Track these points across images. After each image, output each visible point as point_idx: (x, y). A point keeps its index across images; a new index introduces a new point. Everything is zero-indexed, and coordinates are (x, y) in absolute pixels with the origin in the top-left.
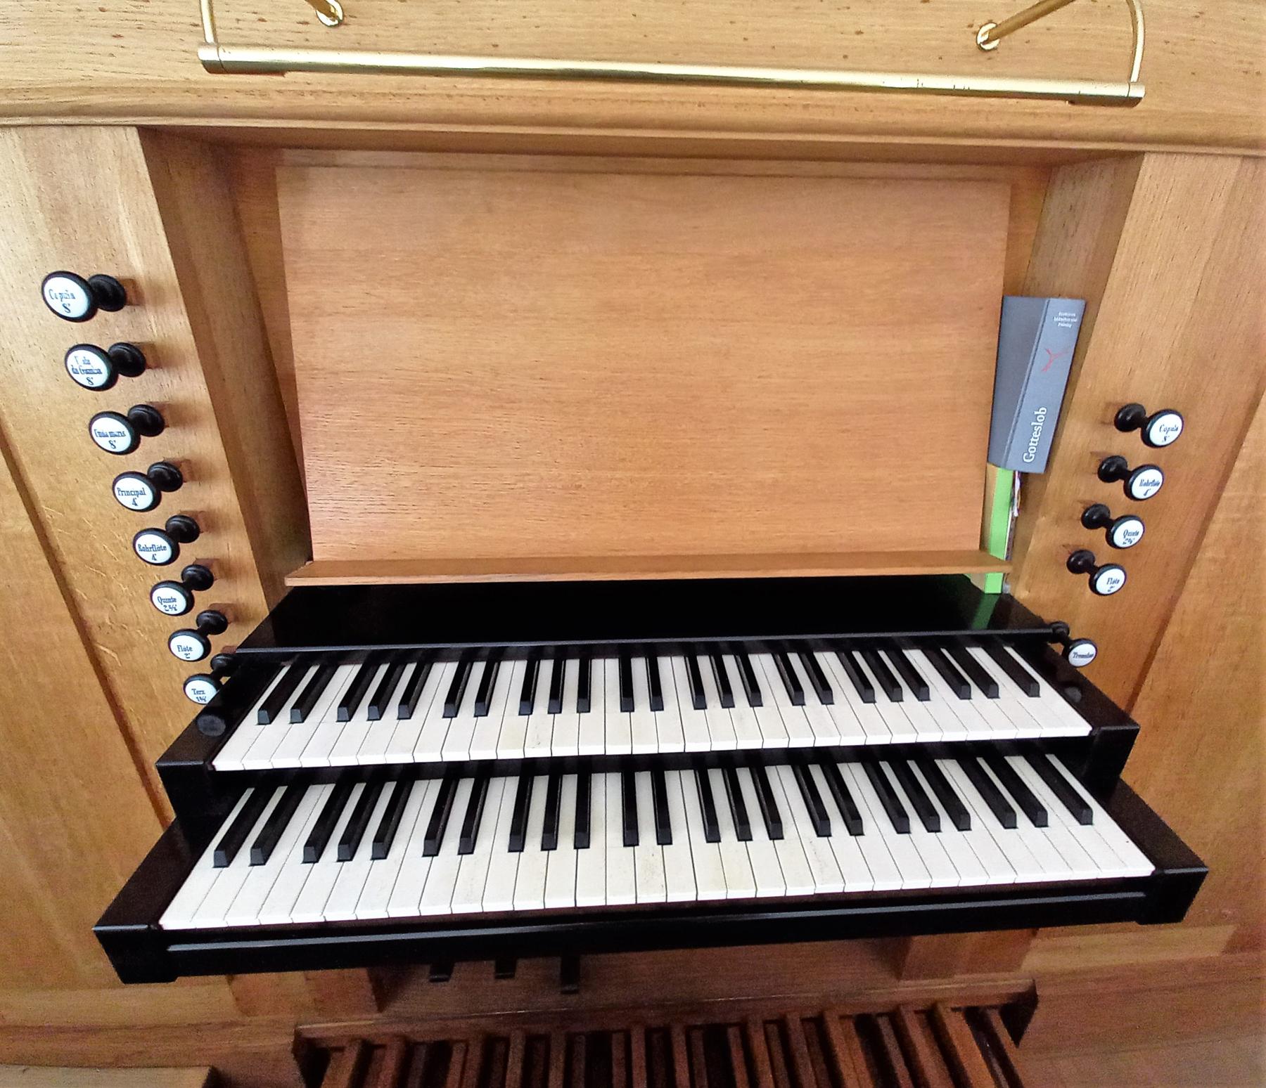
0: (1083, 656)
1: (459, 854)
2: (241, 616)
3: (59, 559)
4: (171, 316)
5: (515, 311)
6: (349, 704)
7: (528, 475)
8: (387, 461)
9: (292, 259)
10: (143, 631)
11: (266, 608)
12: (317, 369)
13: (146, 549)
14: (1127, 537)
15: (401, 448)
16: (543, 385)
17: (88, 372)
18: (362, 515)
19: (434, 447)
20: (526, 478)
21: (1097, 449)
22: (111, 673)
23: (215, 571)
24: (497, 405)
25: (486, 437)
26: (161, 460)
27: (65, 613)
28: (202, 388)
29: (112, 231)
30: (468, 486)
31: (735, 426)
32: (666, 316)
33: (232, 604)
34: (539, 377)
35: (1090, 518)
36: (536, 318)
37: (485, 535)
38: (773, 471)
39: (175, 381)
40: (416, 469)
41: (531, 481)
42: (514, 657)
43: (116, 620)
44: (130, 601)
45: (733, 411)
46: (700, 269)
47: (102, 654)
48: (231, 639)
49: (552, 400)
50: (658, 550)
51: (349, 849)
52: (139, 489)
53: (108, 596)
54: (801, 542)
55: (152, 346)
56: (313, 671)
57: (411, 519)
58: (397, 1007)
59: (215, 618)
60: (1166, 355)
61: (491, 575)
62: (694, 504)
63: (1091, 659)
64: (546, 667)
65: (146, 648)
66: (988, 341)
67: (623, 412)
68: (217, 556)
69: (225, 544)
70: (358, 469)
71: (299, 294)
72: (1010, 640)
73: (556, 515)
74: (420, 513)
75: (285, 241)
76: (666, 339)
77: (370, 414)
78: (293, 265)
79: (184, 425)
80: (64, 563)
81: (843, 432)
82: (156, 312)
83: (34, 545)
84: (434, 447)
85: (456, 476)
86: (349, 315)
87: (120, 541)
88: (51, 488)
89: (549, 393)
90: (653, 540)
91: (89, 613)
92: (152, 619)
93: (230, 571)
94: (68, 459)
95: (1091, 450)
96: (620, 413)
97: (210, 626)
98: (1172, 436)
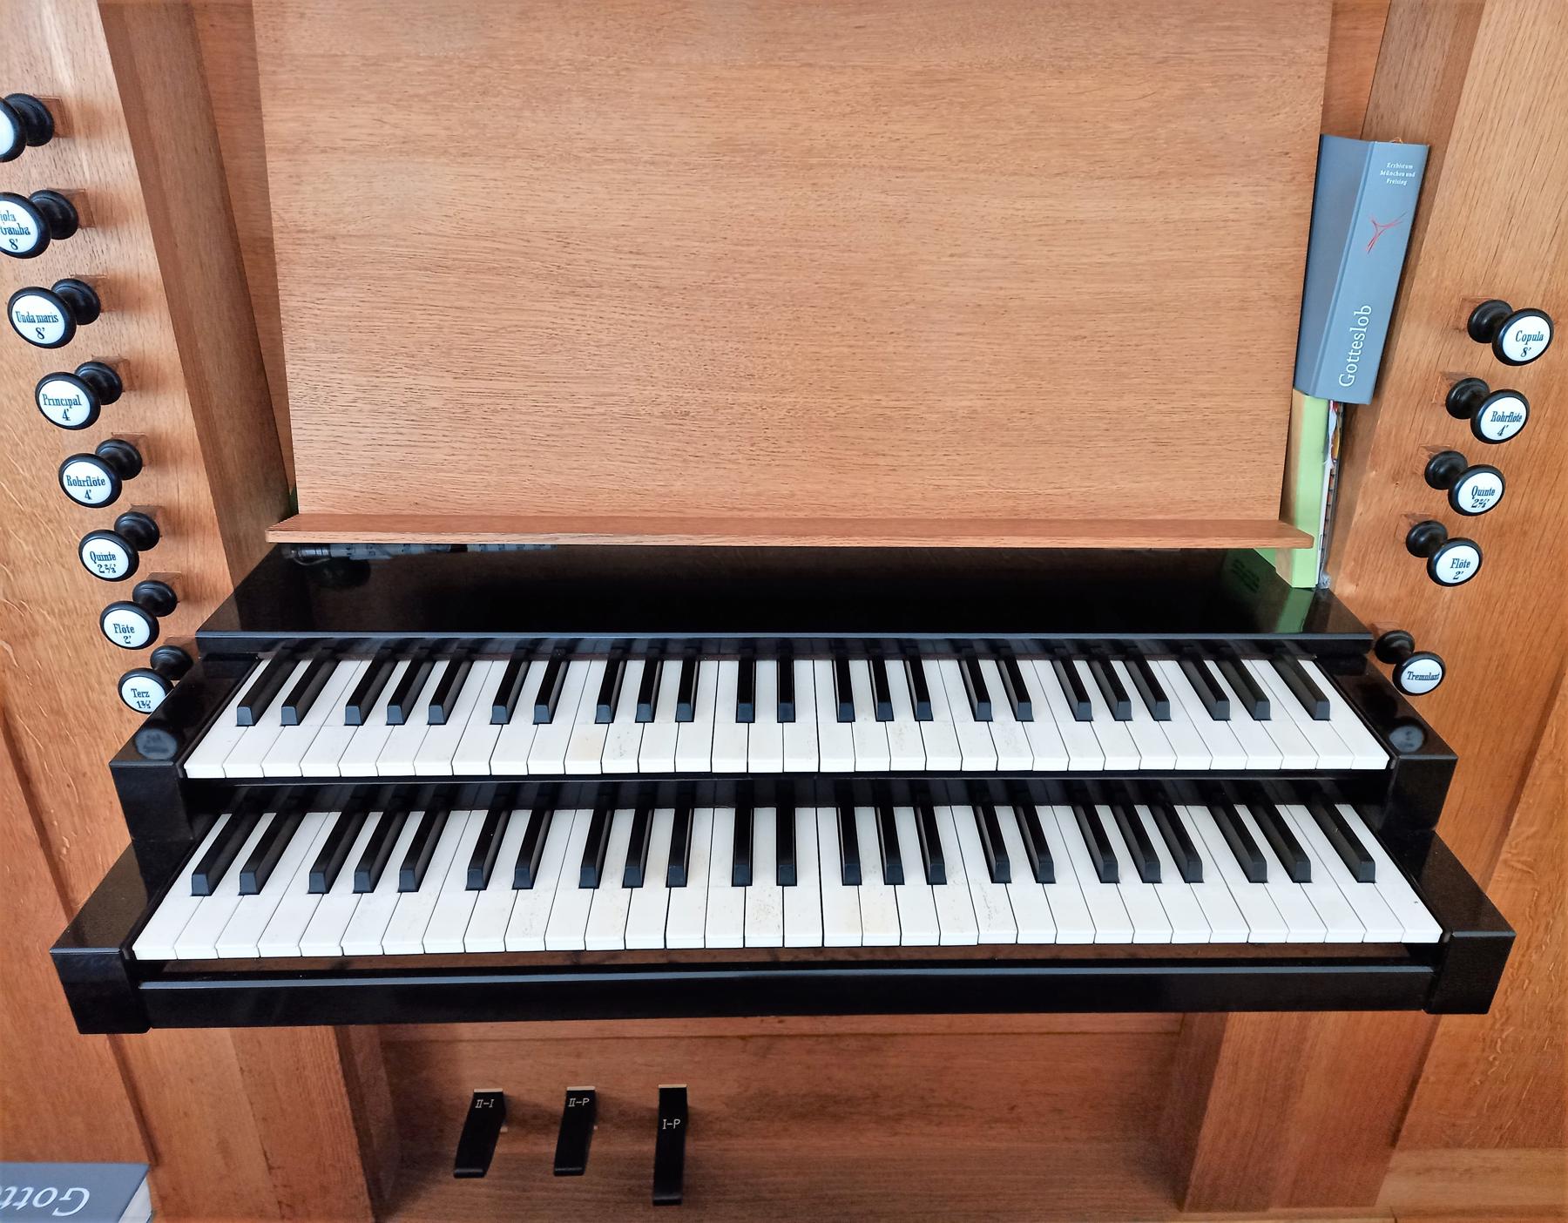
0: (1422, 678)
1: (513, 888)
2: (195, 597)
4: (110, 154)
5: (594, 149)
6: (361, 702)
9: (269, 68)
10: (51, 613)
11: (230, 581)
12: (306, 232)
13: (78, 483)
15: (427, 350)
16: (635, 263)
18: (369, 448)
20: (610, 400)
21: (1452, 369)
25: (550, 337)
26: (90, 359)
28: (150, 257)
29: (31, 31)
32: (814, 161)
33: (181, 575)
35: (1434, 472)
36: (624, 161)
38: (971, 397)
39: (113, 247)
40: (449, 382)
42: (590, 656)
43: (14, 595)
44: (35, 566)
45: (912, 306)
46: (867, 90)
48: (182, 626)
49: (646, 284)
50: (800, 510)
51: (368, 879)
52: (73, 397)
54: (1010, 503)
55: (83, 195)
56: (303, 667)
57: (439, 456)
59: (162, 593)
60: (1549, 228)
63: (1436, 682)
64: (634, 671)
65: (54, 639)
66: (1296, 203)
67: (752, 306)
68: (161, 502)
69: (173, 484)
70: (363, 380)
71: (279, 120)
72: (1307, 649)
75: (260, 44)
76: (815, 196)
77: (382, 299)
78: (273, 77)
79: (123, 311)
81: (1076, 339)
82: (89, 146)
84: (475, 350)
85: (505, 394)
86: (352, 153)
87: (25, 478)
89: (642, 274)
90: (793, 495)
92: (65, 595)
93: (181, 526)
95: (1441, 369)
96: (746, 307)
98: (1536, 348)
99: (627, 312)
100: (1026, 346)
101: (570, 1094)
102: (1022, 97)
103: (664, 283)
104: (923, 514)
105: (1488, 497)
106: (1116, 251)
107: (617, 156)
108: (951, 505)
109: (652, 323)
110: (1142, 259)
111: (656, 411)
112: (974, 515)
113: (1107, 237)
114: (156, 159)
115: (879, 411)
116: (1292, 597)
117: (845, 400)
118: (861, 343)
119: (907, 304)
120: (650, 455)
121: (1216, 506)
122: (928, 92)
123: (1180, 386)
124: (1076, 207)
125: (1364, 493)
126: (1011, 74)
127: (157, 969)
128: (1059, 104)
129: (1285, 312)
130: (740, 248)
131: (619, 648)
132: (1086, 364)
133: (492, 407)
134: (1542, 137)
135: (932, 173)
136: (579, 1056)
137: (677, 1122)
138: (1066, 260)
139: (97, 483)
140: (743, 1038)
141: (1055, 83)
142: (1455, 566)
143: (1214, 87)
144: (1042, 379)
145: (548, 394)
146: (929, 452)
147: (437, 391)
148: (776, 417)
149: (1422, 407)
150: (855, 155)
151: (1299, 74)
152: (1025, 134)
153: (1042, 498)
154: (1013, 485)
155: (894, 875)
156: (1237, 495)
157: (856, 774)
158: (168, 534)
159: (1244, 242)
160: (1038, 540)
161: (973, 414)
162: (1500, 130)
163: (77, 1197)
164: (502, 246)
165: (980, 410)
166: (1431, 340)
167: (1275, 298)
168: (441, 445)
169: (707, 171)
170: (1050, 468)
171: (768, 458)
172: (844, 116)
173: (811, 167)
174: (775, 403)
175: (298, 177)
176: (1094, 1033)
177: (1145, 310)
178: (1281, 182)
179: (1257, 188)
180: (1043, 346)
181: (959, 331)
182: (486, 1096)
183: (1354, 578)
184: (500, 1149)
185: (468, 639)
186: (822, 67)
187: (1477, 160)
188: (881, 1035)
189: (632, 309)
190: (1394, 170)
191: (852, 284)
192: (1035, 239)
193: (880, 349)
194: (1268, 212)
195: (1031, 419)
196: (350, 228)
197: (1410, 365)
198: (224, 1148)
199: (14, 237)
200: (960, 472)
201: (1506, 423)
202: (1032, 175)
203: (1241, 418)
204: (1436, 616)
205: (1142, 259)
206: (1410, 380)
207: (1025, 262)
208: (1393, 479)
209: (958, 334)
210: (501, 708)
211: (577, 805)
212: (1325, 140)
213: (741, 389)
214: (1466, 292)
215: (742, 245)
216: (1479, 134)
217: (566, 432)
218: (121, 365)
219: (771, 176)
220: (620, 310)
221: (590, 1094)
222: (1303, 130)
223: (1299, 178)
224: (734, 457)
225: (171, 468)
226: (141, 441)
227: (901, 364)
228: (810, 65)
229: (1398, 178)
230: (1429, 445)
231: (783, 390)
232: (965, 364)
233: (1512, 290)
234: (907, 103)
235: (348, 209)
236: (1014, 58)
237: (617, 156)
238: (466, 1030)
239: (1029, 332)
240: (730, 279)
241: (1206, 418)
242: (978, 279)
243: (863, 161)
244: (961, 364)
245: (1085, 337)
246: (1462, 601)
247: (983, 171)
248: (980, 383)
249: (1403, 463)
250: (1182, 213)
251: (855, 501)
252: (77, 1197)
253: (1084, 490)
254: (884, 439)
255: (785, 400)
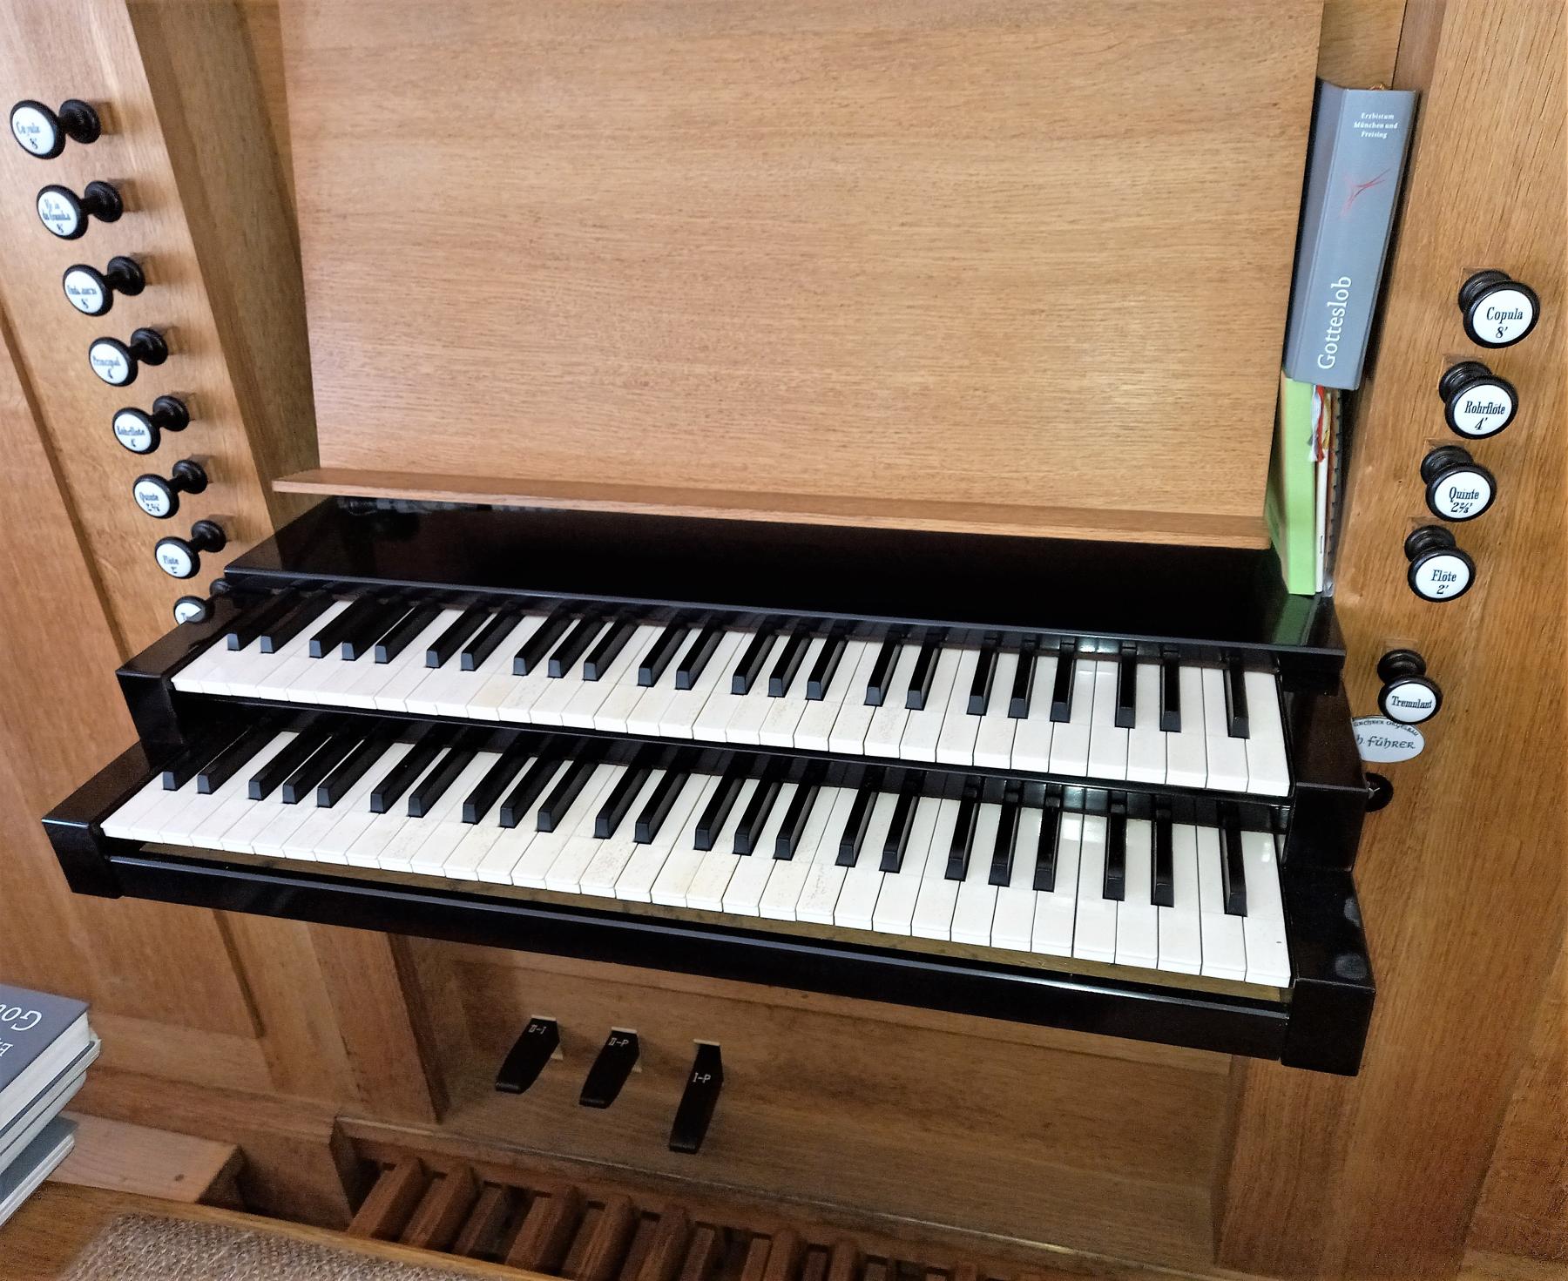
0: (1409, 704)
3: (56, 444)
5: (560, 127)
6: (652, 668)
7: (579, 364)
8: (404, 338)
11: (271, 527)
13: (124, 432)
14: (1455, 500)
15: (420, 320)
16: (598, 236)
17: (57, 218)
19: (460, 320)
20: (576, 369)
22: (114, 595)
23: (210, 470)
24: (539, 263)
25: (524, 308)
27: (62, 511)
30: (502, 376)
31: (865, 300)
32: (765, 130)
34: (590, 223)
37: (523, 445)
38: (922, 373)
40: (438, 350)
41: (582, 373)
42: (868, 637)
43: (116, 527)
45: (862, 278)
47: (104, 569)
49: (608, 256)
50: (753, 483)
52: (114, 360)
53: (106, 497)
54: (963, 485)
55: (131, 183)
57: (432, 418)
58: (454, 1122)
61: (506, 496)
62: (804, 418)
64: (1007, 664)
66: (1286, 161)
67: (706, 278)
70: (370, 347)
73: (616, 424)
74: (443, 411)
76: (766, 166)
80: (61, 450)
81: (1033, 312)
82: (134, 142)
83: (28, 426)
84: (460, 320)
85: (486, 362)
88: (43, 357)
91: (88, 515)
92: (152, 529)
93: (229, 475)
94: (59, 321)
95: (1443, 350)
96: (700, 279)
97: (205, 540)
98: (1515, 329)
99: (591, 284)
100: (980, 320)
101: (615, 1034)
102: (976, 55)
103: (624, 255)
104: (873, 494)
105: (1470, 501)
106: (1078, 217)
107: (581, 132)
108: (902, 485)
109: (614, 295)
110: (1108, 225)
111: (619, 381)
112: (926, 496)
113: (1067, 203)
114: (193, 149)
115: (831, 385)
116: (1289, 604)
117: (796, 374)
118: (811, 316)
119: (858, 275)
120: (612, 423)
121: (1190, 498)
122: (877, 54)
123: (1148, 365)
124: (1034, 171)
125: (1361, 491)
126: (965, 31)
127: (132, 847)
128: (1015, 61)
129: (1273, 285)
130: (693, 220)
131: (804, 625)
132: (1045, 340)
133: (476, 374)
134: (1551, 77)
135: (882, 139)
136: (620, 998)
137: (707, 1077)
138: (1023, 228)
139: (140, 433)
140: (769, 1007)
141: (1012, 38)
142: (1437, 578)
143: (1189, 33)
144: (997, 355)
145: (522, 363)
146: (880, 429)
147: (429, 357)
148: (729, 389)
149: (1424, 395)
150: (805, 122)
151: (1290, 13)
152: (980, 95)
153: (995, 482)
154: (966, 466)
155: (1001, 874)
156: (1214, 487)
157: (936, 765)
158: (219, 479)
159: (1225, 205)
160: (1247, 540)
161: (925, 390)
162: (1494, 70)
163: (33, 1017)
164: (484, 222)
165: (932, 387)
166: (1428, 317)
167: (1260, 269)
168: (433, 408)
169: (663, 143)
170: (1006, 450)
171: (721, 430)
172: (794, 83)
173: (762, 136)
174: (729, 375)
175: (316, 161)
176: (1130, 1061)
177: (1109, 282)
178: (1268, 136)
179: (1239, 145)
180: (998, 320)
181: (911, 303)
182: (540, 1023)
183: (1357, 587)
184: (628, 1088)
185: (937, 627)
186: (772, 35)
187: (1468, 105)
188: (905, 1027)
189: (596, 281)
190: (1369, 121)
191: (802, 255)
192: (991, 205)
193: (830, 323)
194: (1253, 171)
195: (985, 397)
196: (359, 206)
197: (1403, 346)
198: (312, 1027)
199: (60, 222)
200: (912, 451)
201: (1485, 416)
202: (986, 138)
203: (1219, 402)
204: (1464, 635)
205: (1108, 225)
206: (1406, 362)
207: (978, 230)
208: (1395, 476)
209: (909, 307)
210: (777, 681)
211: (841, 783)
212: (1328, 92)
213: (695, 360)
214: (1468, 261)
215: (697, 217)
216: (1467, 75)
217: (539, 399)
218: (171, 331)
219: (722, 147)
220: (584, 282)
221: (632, 1037)
222: (1295, 77)
223: (1291, 131)
224: (690, 428)
225: (218, 423)
226: (191, 398)
227: (851, 338)
228: (760, 33)
229: (1376, 130)
230: (1437, 439)
231: (736, 363)
232: (917, 338)
233: (1529, 257)
234: (857, 67)
235: (355, 190)
236: (967, 13)
237: (581, 132)
238: (523, 959)
239: (984, 305)
240: (685, 252)
241: (1179, 401)
242: (930, 249)
243: (812, 129)
244: (912, 338)
245: (1043, 311)
246: (1497, 622)
247: (936, 135)
248: (933, 358)
249: (1406, 458)
250: (1153, 175)
251: (806, 476)
252: (33, 1017)
253: (1042, 474)
254: (834, 414)
255: (739, 373)
